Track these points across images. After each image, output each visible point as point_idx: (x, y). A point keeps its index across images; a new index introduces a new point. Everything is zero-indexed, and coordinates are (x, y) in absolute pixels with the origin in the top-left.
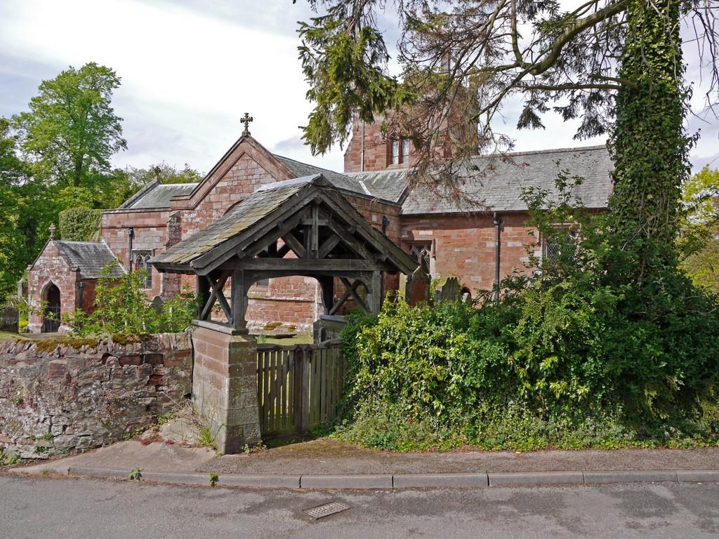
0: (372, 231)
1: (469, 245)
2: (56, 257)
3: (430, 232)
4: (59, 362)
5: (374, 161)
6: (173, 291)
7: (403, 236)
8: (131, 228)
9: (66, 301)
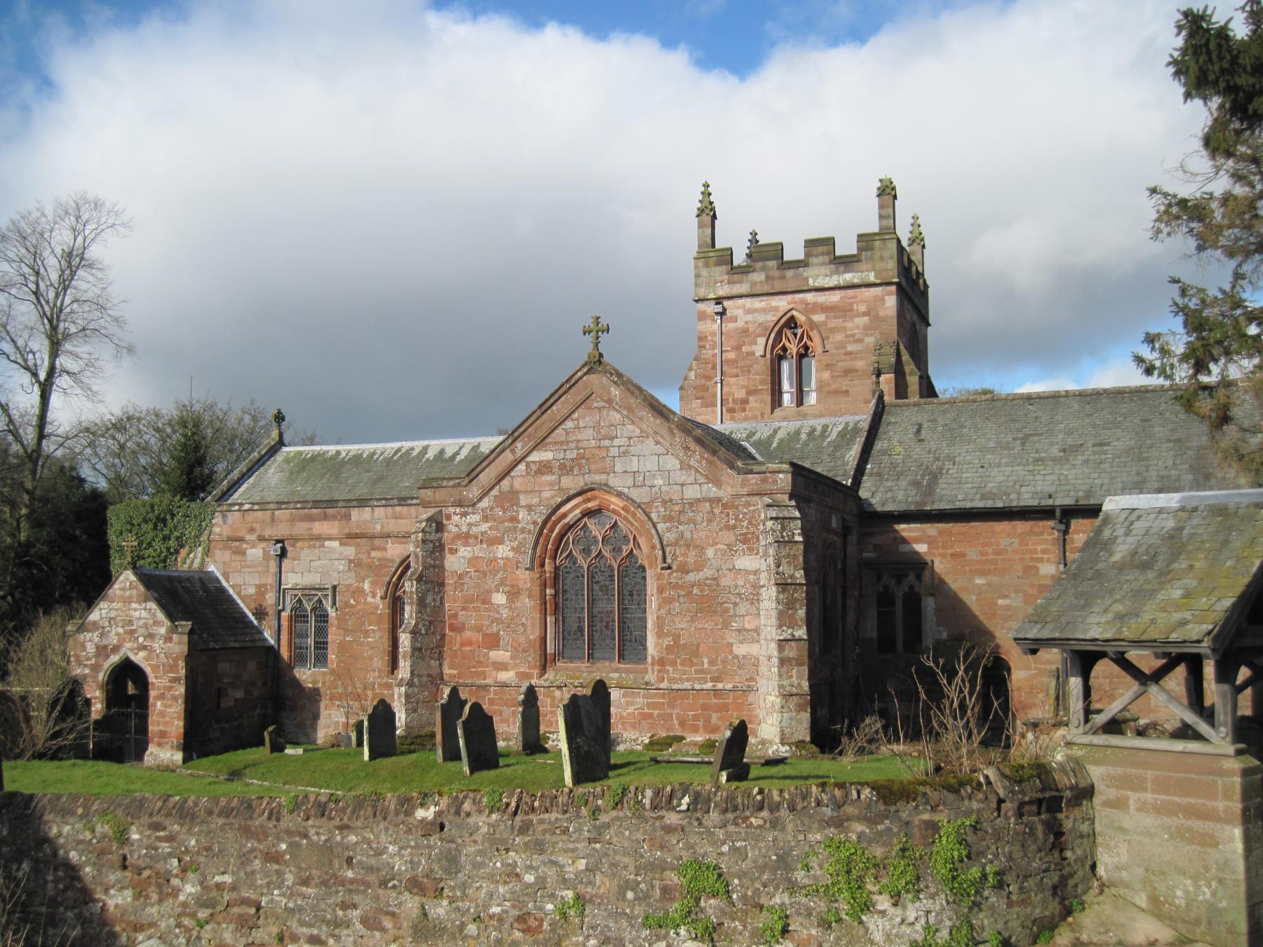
2: (139, 602)
5: (745, 402)
6: (429, 676)
7: (865, 555)
8: (278, 541)
9: (161, 697)
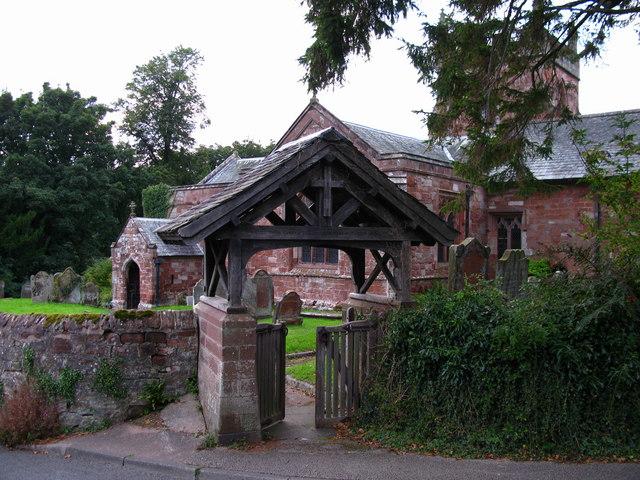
0: (399, 193)
1: (564, 217)
3: (521, 203)
4: (64, 337)
9: (144, 278)
